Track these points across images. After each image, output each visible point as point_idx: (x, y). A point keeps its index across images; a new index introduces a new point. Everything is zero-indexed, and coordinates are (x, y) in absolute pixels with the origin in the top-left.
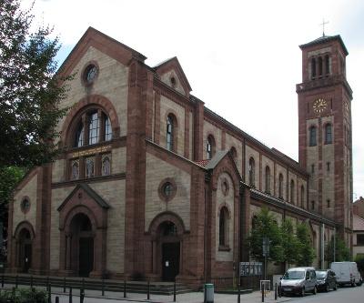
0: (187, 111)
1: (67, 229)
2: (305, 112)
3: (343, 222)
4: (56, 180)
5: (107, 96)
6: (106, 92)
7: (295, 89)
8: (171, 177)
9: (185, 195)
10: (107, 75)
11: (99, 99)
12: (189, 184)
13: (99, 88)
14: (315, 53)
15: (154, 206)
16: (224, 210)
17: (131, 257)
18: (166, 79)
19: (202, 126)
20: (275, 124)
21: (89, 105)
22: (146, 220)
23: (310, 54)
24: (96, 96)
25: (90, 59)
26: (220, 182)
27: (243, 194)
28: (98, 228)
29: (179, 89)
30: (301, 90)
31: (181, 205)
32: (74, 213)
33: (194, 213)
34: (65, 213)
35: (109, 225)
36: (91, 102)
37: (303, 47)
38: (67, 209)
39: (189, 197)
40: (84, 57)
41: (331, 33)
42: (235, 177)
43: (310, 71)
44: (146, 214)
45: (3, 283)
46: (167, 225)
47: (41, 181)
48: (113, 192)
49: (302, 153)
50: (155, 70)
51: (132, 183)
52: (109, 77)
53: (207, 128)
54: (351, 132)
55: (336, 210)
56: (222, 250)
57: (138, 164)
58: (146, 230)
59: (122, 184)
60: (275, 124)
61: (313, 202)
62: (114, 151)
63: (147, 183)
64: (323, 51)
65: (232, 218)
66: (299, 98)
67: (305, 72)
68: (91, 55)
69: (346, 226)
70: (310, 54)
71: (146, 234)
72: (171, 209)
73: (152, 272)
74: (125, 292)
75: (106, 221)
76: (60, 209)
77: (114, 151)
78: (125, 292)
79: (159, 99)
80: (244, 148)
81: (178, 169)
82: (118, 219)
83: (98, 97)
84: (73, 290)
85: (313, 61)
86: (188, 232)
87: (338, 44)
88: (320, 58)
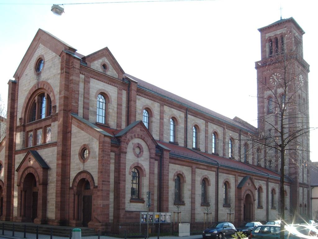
0: (120, 90)
1: (22, 186)
2: (263, 83)
3: (296, 178)
4: (18, 148)
5: (49, 81)
6: (48, 79)
7: (254, 66)
8: (86, 143)
9: (95, 158)
10: (50, 65)
11: (44, 85)
12: (98, 149)
13: (44, 76)
14: (271, 34)
15: (76, 167)
16: (138, 169)
17: (61, 206)
18: (96, 65)
19: (135, 102)
20: (237, 98)
21: (39, 89)
22: (71, 178)
23: (268, 35)
24: (43, 81)
25: (39, 54)
26: (131, 145)
27: (160, 152)
28: (40, 184)
29: (111, 72)
30: (259, 66)
31: (92, 166)
32: (26, 173)
33: (101, 172)
34: (21, 173)
35: (49, 182)
36: (40, 87)
37: (261, 30)
38: (22, 170)
39: (97, 159)
40: (36, 52)
41: (286, 17)
42: (150, 142)
43: (267, 50)
44: (71, 173)
45: (3, 229)
46: (84, 182)
47: (8, 149)
48: (50, 156)
49: (261, 120)
50: (84, 58)
51: (60, 148)
52: (51, 67)
53: (141, 102)
54: (307, 100)
55: (290, 168)
56: (273, 209)
57: (66, 134)
58: (71, 186)
59: (55, 149)
60: (237, 98)
61: (270, 161)
62: (52, 124)
63: (72, 149)
64: (278, 32)
65: (148, 176)
66: (258, 73)
67: (263, 51)
68: (41, 51)
69: (300, 180)
70: (268, 35)
71: (70, 188)
72: (86, 169)
73: (74, 219)
74: (25, 232)
75: (47, 179)
76: (17, 170)
77: (52, 124)
78: (25, 232)
79: (89, 82)
80: (186, 118)
81: (91, 137)
82: (53, 177)
83: (45, 83)
84: (5, 231)
85: (270, 40)
86: (97, 187)
87: (292, 25)
88: (276, 39)
